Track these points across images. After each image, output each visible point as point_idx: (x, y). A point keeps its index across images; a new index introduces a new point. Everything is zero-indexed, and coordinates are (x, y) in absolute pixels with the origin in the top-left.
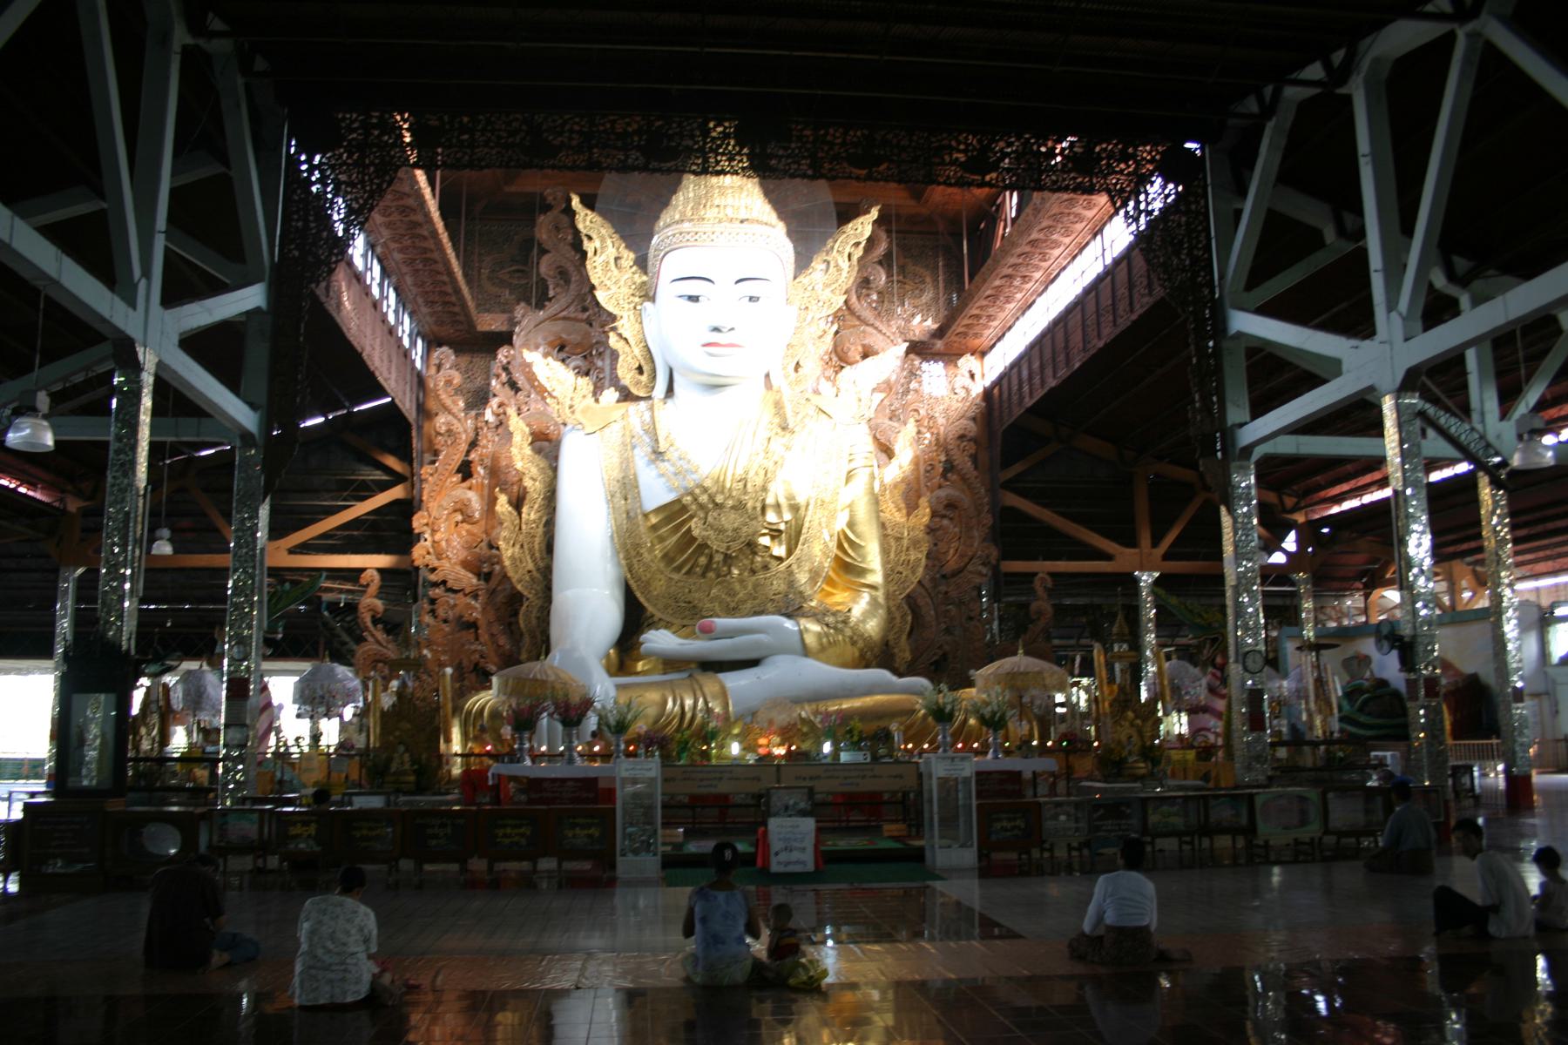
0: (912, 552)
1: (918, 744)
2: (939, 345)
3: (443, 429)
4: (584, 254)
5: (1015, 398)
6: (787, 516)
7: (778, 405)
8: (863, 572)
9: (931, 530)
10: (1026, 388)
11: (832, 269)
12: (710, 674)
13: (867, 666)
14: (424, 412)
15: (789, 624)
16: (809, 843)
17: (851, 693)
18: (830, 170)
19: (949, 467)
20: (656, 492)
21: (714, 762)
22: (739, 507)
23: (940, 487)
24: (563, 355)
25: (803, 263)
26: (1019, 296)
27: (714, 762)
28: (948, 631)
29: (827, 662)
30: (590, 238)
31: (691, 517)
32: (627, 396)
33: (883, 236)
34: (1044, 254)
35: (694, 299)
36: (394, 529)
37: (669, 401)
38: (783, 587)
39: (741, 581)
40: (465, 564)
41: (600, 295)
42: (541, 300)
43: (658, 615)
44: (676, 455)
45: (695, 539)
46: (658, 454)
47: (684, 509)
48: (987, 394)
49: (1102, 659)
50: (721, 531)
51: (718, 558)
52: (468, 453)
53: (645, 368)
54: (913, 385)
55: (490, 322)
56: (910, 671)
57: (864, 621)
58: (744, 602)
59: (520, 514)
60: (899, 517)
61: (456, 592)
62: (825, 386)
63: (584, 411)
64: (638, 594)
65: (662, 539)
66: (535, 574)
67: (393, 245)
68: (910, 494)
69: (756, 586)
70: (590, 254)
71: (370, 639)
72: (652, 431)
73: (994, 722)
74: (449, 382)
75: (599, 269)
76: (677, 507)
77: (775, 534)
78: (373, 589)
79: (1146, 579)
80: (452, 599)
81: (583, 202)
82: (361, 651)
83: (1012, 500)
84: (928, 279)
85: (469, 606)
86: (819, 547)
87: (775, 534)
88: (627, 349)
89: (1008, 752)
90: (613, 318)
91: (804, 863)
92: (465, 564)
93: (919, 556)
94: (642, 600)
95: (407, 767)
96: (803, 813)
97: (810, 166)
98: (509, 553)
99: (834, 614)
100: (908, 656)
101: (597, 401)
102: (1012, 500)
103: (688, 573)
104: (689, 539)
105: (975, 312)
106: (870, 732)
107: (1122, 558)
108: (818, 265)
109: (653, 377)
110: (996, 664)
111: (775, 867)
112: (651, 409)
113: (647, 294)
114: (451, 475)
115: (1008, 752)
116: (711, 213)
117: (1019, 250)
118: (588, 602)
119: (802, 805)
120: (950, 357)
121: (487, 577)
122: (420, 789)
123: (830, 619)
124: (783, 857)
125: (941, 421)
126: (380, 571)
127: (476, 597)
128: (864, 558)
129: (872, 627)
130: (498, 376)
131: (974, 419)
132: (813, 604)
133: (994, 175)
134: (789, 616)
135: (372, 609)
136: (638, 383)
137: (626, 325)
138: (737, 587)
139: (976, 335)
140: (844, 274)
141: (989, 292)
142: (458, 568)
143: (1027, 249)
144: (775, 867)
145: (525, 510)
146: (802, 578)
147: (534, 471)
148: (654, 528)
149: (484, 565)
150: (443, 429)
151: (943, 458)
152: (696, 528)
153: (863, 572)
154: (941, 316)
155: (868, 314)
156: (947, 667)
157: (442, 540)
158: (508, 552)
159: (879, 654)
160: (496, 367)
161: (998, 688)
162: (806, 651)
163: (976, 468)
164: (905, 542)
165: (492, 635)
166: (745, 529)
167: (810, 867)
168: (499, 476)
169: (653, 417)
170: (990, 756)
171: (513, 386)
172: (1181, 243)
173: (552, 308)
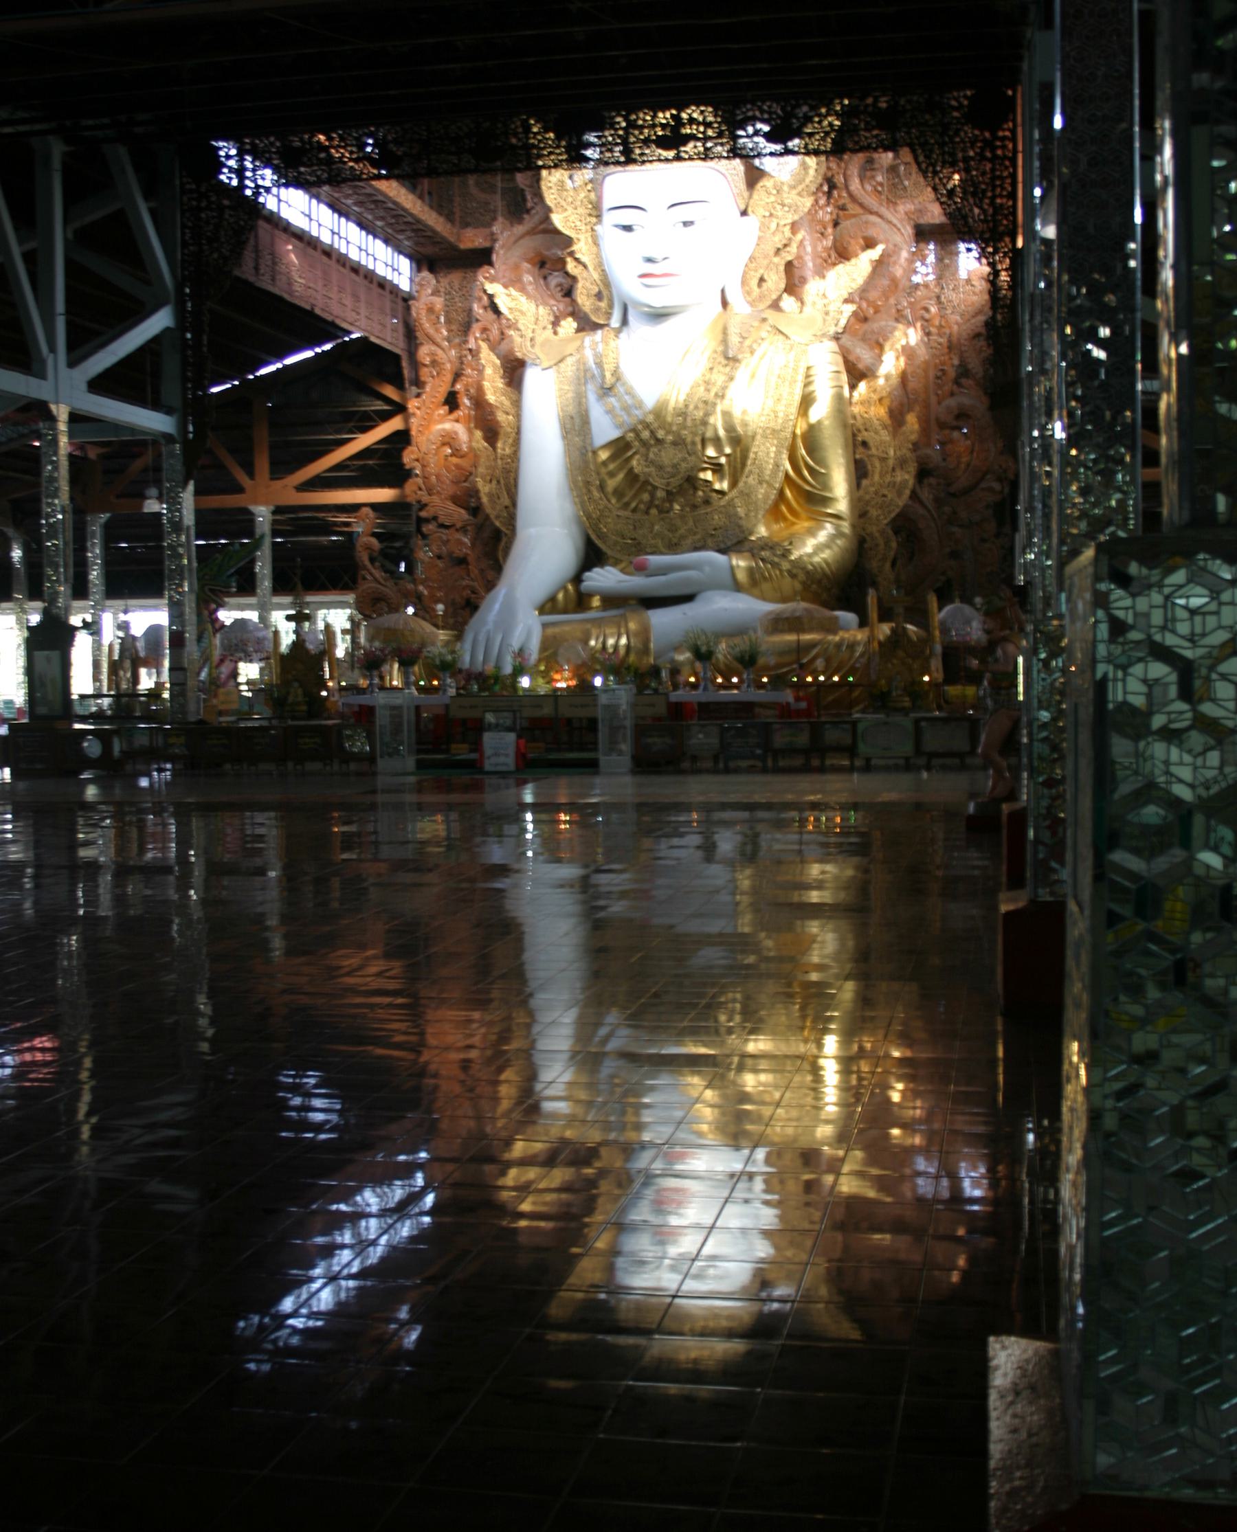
1: (727, 679)
6: (728, 450)
8: (826, 501)
15: (720, 558)
16: (511, 751)
18: (642, 154)
19: (963, 372)
20: (604, 430)
22: (679, 443)
23: (952, 394)
24: (545, 271)
28: (954, 555)
31: (635, 453)
35: (628, 228)
39: (682, 517)
40: (455, 500)
41: (557, 220)
43: (609, 552)
51: (660, 494)
52: (454, 381)
53: (605, 293)
55: (472, 239)
58: (683, 537)
59: (494, 448)
61: (447, 527)
63: (543, 345)
65: (612, 475)
71: (368, 577)
74: (431, 310)
85: (460, 543)
87: (717, 469)
90: (569, 241)
91: (506, 765)
95: (300, 699)
97: (622, 153)
101: (555, 333)
104: (632, 477)
114: (438, 407)
118: (546, 542)
122: (311, 715)
124: (494, 760)
127: (463, 530)
128: (830, 489)
133: (796, 141)
134: (722, 551)
135: (368, 548)
136: (597, 310)
137: (582, 248)
138: (678, 522)
140: (812, 172)
145: (499, 445)
148: (604, 463)
149: (468, 500)
150: (427, 361)
151: (956, 362)
153: (826, 501)
155: (871, 201)
158: (484, 488)
159: (844, 587)
162: (737, 587)
164: (891, 462)
165: (482, 571)
166: (684, 465)
167: (512, 767)
172: (984, 192)
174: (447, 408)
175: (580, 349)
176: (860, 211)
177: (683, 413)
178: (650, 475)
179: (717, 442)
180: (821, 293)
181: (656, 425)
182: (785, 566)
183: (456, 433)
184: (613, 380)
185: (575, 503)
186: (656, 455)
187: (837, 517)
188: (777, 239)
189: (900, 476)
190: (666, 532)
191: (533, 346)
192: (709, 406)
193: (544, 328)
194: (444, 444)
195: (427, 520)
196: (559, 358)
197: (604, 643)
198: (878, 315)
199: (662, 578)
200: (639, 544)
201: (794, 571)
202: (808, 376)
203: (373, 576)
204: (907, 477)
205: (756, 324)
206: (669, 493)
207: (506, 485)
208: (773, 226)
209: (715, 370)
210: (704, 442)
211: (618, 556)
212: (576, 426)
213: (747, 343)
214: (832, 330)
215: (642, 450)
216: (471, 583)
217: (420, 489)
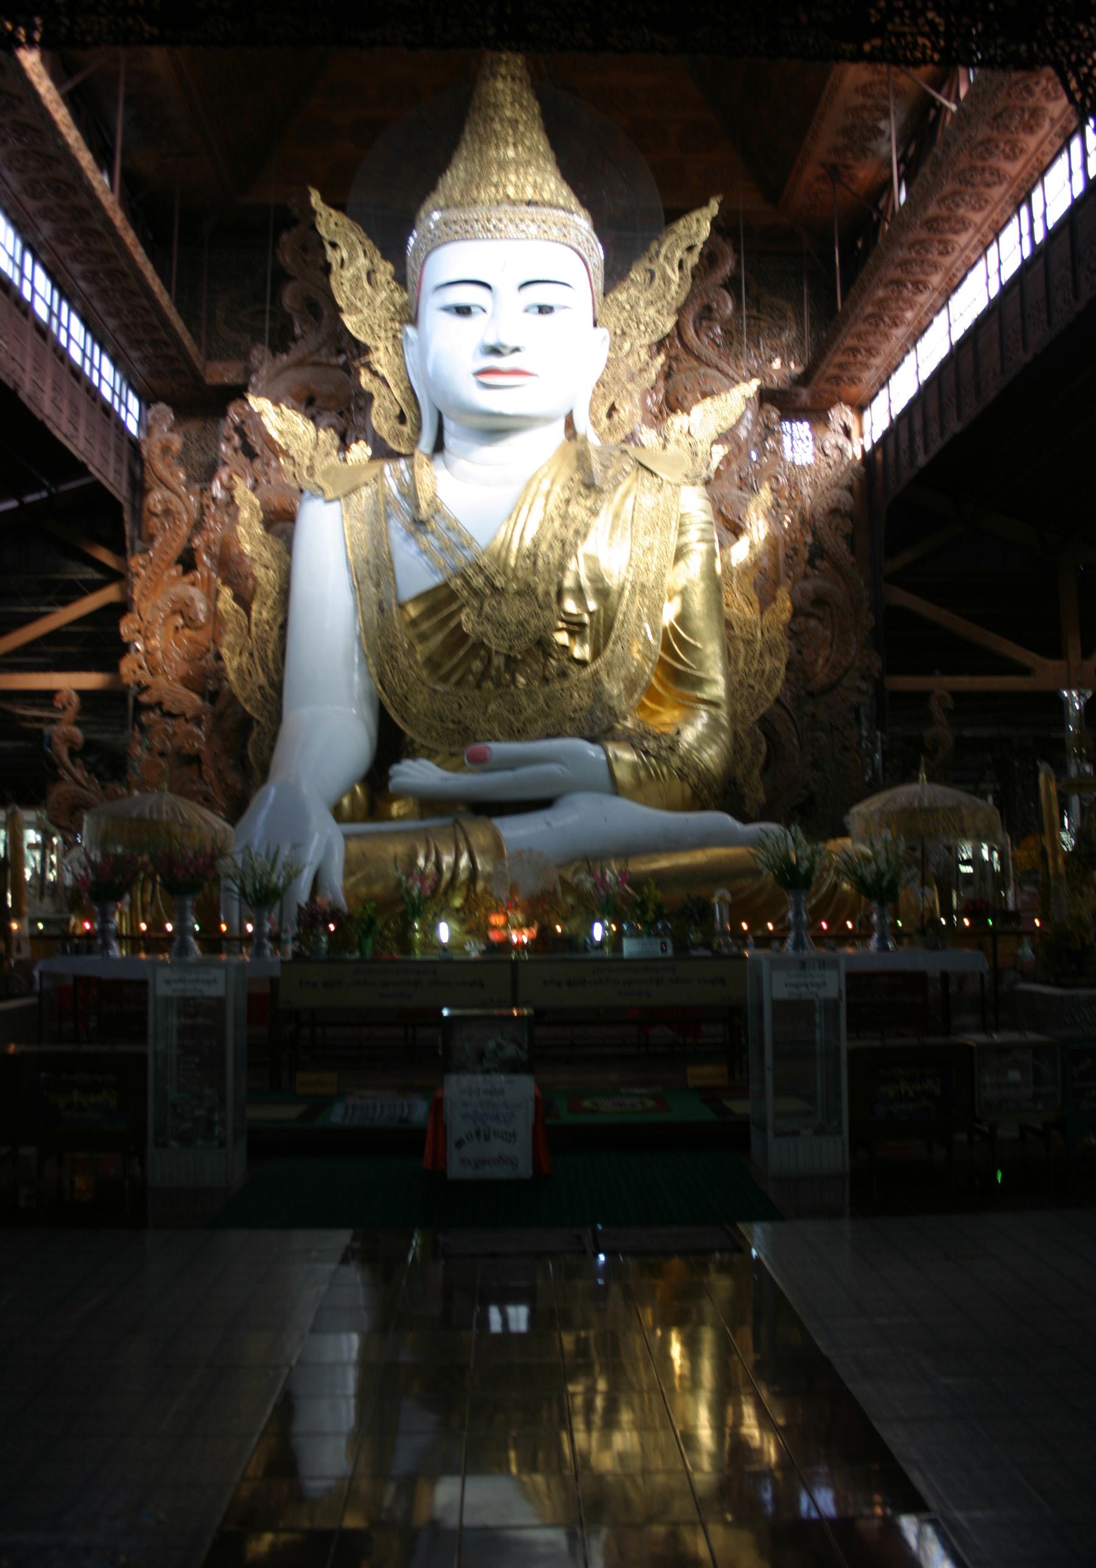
0: (767, 659)
1: (757, 923)
2: (804, 395)
3: (159, 508)
4: (327, 268)
5: (904, 458)
6: (592, 605)
7: (582, 459)
8: (698, 683)
9: (793, 633)
10: (919, 441)
11: (657, 280)
12: (483, 819)
13: (704, 807)
14: (139, 488)
15: (592, 751)
16: (523, 1124)
17: (674, 844)
19: (818, 552)
20: (416, 573)
21: (418, 955)
22: (527, 592)
23: (806, 576)
24: (313, 410)
25: (614, 274)
26: (909, 315)
27: (418, 955)
29: (646, 803)
30: (334, 245)
31: (462, 606)
32: (382, 452)
33: (728, 250)
34: (945, 243)
36: (99, 642)
37: (439, 460)
38: (586, 701)
39: (529, 693)
40: (187, 682)
41: (349, 321)
42: (281, 342)
43: (419, 740)
44: (443, 525)
45: (466, 636)
46: (419, 524)
47: (453, 596)
48: (868, 458)
49: (1053, 788)
50: (501, 625)
51: (498, 661)
54: (770, 443)
55: (221, 373)
56: (765, 815)
57: (699, 748)
58: (531, 721)
59: (248, 610)
60: (750, 614)
62: (648, 436)
63: (326, 474)
64: (392, 713)
65: (423, 637)
66: (268, 690)
67: (63, 250)
68: (765, 579)
69: (549, 699)
70: (335, 267)
71: (66, 777)
72: (410, 493)
73: (880, 890)
74: (166, 449)
75: (347, 287)
76: (443, 593)
77: (576, 628)
78: (71, 713)
79: (1075, 700)
80: (170, 725)
81: (327, 200)
82: (56, 792)
83: (900, 597)
84: (790, 314)
85: (190, 735)
86: (638, 647)
87: (576, 628)
88: (384, 390)
89: (899, 935)
90: (362, 349)
92: (187, 682)
93: (776, 665)
94: (397, 720)
96: (513, 1067)
98: (235, 663)
99: (656, 738)
100: (762, 797)
102: (900, 597)
103: (459, 683)
104: (458, 637)
105: (850, 342)
106: (674, 907)
107: (1044, 671)
108: (637, 275)
109: (418, 428)
110: (885, 796)
111: (456, 1170)
112: (411, 468)
113: (410, 315)
114: (169, 566)
115: (899, 935)
116: (487, 194)
117: (911, 236)
118: (328, 723)
119: (511, 1050)
120: (817, 415)
121: (212, 697)
123: (650, 745)
125: (807, 491)
126: (82, 694)
127: (197, 721)
128: (701, 665)
129: (711, 756)
130: (229, 440)
131: (850, 489)
132: (629, 724)
133: (877, 42)
134: (592, 740)
135: (69, 740)
137: (382, 359)
138: (524, 701)
139: (853, 381)
140: (674, 288)
141: (869, 310)
142: (180, 688)
143: (923, 234)
144: (456, 1170)
145: (255, 607)
146: (614, 688)
147: (267, 555)
148: (414, 623)
149: (207, 681)
150: (159, 508)
152: (467, 619)
154: (806, 361)
155: (710, 353)
156: (820, 817)
157: (156, 646)
158: (232, 663)
159: (720, 792)
160: (226, 428)
161: (887, 834)
162: (615, 788)
163: (853, 552)
164: (758, 647)
165: (220, 773)
166: (533, 622)
168: (230, 567)
169: (413, 477)
170: (873, 943)
171: (249, 452)
173: (297, 351)
174: (180, 568)
175: (379, 477)
176: (695, 363)
177: (533, 556)
178: (485, 634)
179: (579, 593)
180: (685, 430)
181: (493, 570)
182: (675, 762)
183: (192, 599)
184: (431, 511)
185: (370, 674)
186: (493, 608)
187: (712, 703)
188: (630, 362)
189: (768, 664)
190: (505, 713)
191: (311, 475)
192: (567, 549)
193: (327, 454)
194: (174, 612)
195: (150, 707)
196: (348, 488)
197: (438, 864)
198: (719, 482)
199: (508, 775)
200: (466, 729)
201: (686, 770)
202: (681, 525)
203: (75, 777)
204: (777, 664)
205: (617, 453)
206: (508, 658)
207: (261, 659)
208: (627, 346)
209: (573, 502)
210: (560, 594)
211: (432, 745)
212: (374, 572)
213: (611, 472)
214: (704, 474)
215: (476, 603)
216: (204, 787)
217: (141, 667)
